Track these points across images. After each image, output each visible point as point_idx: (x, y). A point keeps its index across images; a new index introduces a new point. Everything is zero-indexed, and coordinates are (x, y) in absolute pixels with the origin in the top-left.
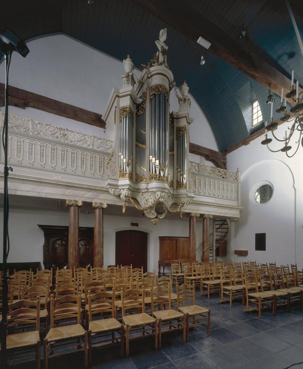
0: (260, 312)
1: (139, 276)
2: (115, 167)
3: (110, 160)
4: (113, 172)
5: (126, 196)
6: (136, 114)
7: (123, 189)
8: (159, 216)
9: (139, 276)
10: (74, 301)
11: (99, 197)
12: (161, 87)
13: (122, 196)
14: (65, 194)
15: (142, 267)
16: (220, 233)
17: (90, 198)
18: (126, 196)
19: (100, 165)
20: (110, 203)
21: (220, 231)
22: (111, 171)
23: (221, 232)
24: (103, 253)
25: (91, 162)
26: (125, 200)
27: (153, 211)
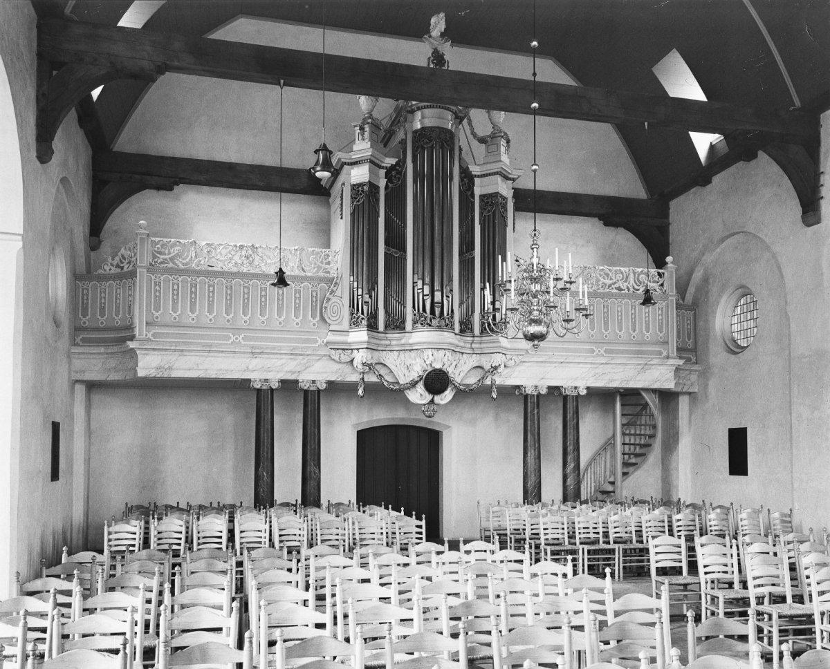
0: (574, 556)
1: (416, 538)
2: (341, 305)
3: (333, 292)
4: (338, 317)
5: (364, 364)
6: (385, 188)
7: (358, 349)
8: (437, 399)
9: (416, 538)
10: (580, 626)
11: (312, 369)
12: (505, 210)
13: (355, 363)
14: (250, 367)
15: (383, 503)
16: (632, 447)
17: (294, 373)
18: (364, 364)
19: (314, 304)
20: (333, 378)
21: (632, 442)
22: (334, 315)
23: (635, 435)
24: (320, 479)
25: (297, 301)
26: (362, 371)
27: (420, 388)
